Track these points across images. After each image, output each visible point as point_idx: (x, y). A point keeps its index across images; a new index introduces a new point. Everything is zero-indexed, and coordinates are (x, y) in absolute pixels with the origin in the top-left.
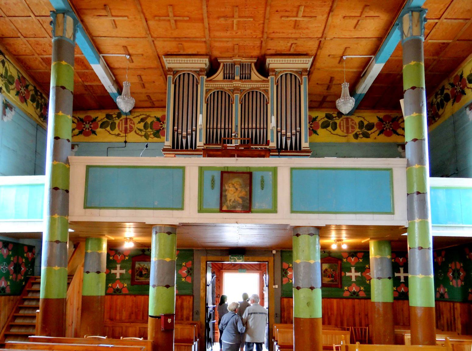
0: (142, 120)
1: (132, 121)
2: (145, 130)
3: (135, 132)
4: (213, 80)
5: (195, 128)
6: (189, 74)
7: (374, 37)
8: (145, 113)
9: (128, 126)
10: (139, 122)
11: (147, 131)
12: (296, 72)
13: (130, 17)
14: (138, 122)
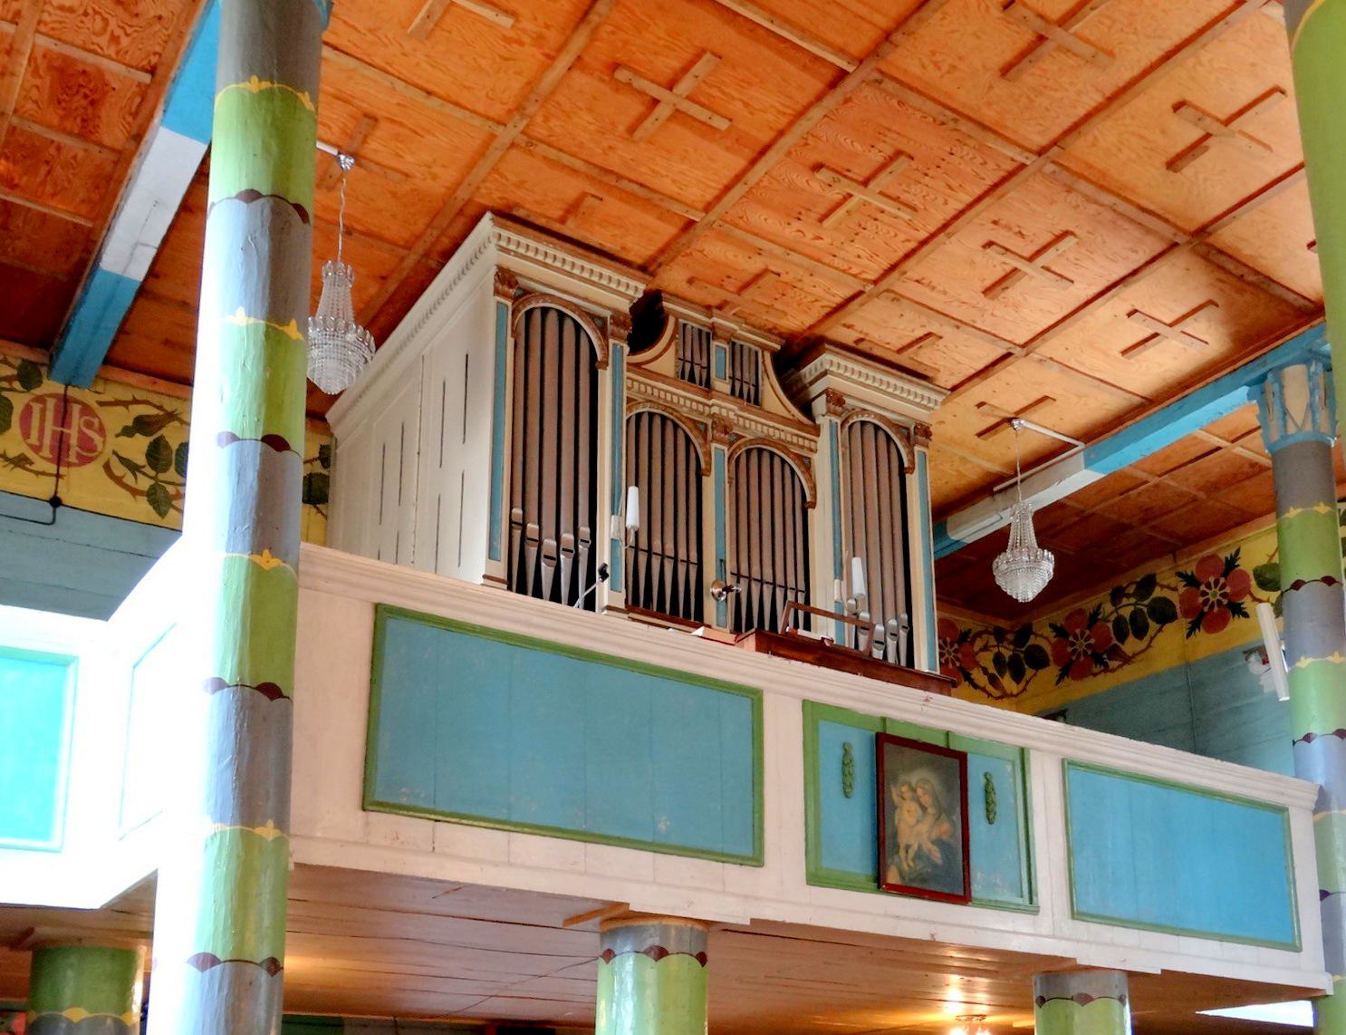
0: (142, 425)
1: (95, 415)
2: (152, 473)
3: (107, 467)
4: (643, 366)
5: (588, 530)
6: (562, 316)
7: (1140, 394)
8: (156, 399)
9: (73, 434)
10: (128, 432)
11: (162, 476)
12: (898, 427)
13: (526, 24)
14: (119, 430)
